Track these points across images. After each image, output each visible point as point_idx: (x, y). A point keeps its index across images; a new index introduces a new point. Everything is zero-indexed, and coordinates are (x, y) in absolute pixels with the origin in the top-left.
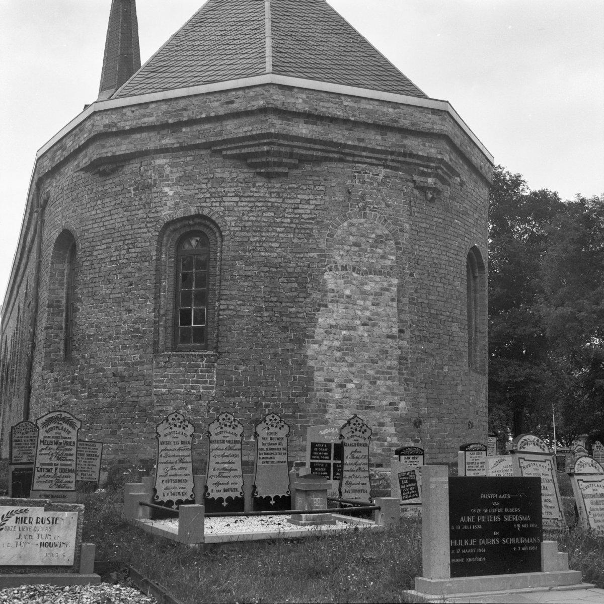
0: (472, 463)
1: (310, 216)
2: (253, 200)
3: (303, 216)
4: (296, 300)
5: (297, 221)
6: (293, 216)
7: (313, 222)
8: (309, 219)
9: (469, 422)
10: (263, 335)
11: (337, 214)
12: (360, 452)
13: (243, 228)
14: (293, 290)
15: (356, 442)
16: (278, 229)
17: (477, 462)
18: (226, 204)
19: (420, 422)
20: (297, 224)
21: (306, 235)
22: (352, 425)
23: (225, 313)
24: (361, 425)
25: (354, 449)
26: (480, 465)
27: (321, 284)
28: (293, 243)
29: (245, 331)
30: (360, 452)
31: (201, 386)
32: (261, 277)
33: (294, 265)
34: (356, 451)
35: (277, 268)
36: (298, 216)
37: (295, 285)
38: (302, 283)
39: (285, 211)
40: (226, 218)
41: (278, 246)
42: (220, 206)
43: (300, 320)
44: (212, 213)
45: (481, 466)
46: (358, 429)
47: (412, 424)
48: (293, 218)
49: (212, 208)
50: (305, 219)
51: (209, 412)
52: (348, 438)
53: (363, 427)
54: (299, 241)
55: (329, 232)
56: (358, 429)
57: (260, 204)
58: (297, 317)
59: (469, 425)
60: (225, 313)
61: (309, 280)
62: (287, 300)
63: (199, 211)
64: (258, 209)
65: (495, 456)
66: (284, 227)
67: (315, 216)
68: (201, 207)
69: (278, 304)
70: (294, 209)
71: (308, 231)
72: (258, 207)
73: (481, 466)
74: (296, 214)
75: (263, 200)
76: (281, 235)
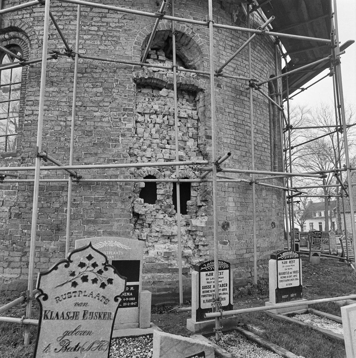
0: (284, 273)
1: (117, 25)
2: (61, 9)
3: (111, 24)
4: (101, 104)
5: (104, 29)
6: (99, 24)
7: (121, 30)
8: (116, 27)
9: (272, 223)
10: (66, 140)
11: (145, 24)
12: (89, 333)
13: (51, 36)
14: (98, 94)
15: (81, 309)
16: (85, 37)
17: (290, 271)
18: (36, 15)
19: (228, 225)
20: (103, 32)
21: (113, 43)
22: (73, 267)
23: (30, 118)
24: (101, 267)
25: (71, 325)
26: (293, 274)
27: (127, 89)
28: (100, 49)
29: (48, 135)
30: (89, 333)
31: (4, 191)
32: (67, 82)
33: (100, 71)
34: (75, 332)
35: (83, 74)
36: (105, 24)
37: (101, 90)
38: (107, 88)
39: (92, 19)
40: (35, 28)
41: (84, 52)
42: (30, 17)
43: (105, 125)
44: (23, 24)
45: (294, 276)
46: (91, 276)
47: (220, 227)
48: (100, 26)
49: (23, 20)
50: (112, 28)
51: (10, 218)
52: (58, 299)
53: (105, 273)
54: (106, 48)
55: (136, 40)
56: (91, 276)
57: (68, 13)
58: (102, 121)
59: (272, 225)
60: (30, 118)
61: (115, 85)
62: (91, 105)
63: (11, 23)
64: (66, 18)
65: (47, 48)
66: (91, 34)
67: (123, 24)
68: (14, 20)
69: (83, 108)
70: (101, 17)
71: (115, 39)
72: (66, 16)
73: (294, 276)
74: (103, 22)
75: (71, 9)
76: (88, 42)
